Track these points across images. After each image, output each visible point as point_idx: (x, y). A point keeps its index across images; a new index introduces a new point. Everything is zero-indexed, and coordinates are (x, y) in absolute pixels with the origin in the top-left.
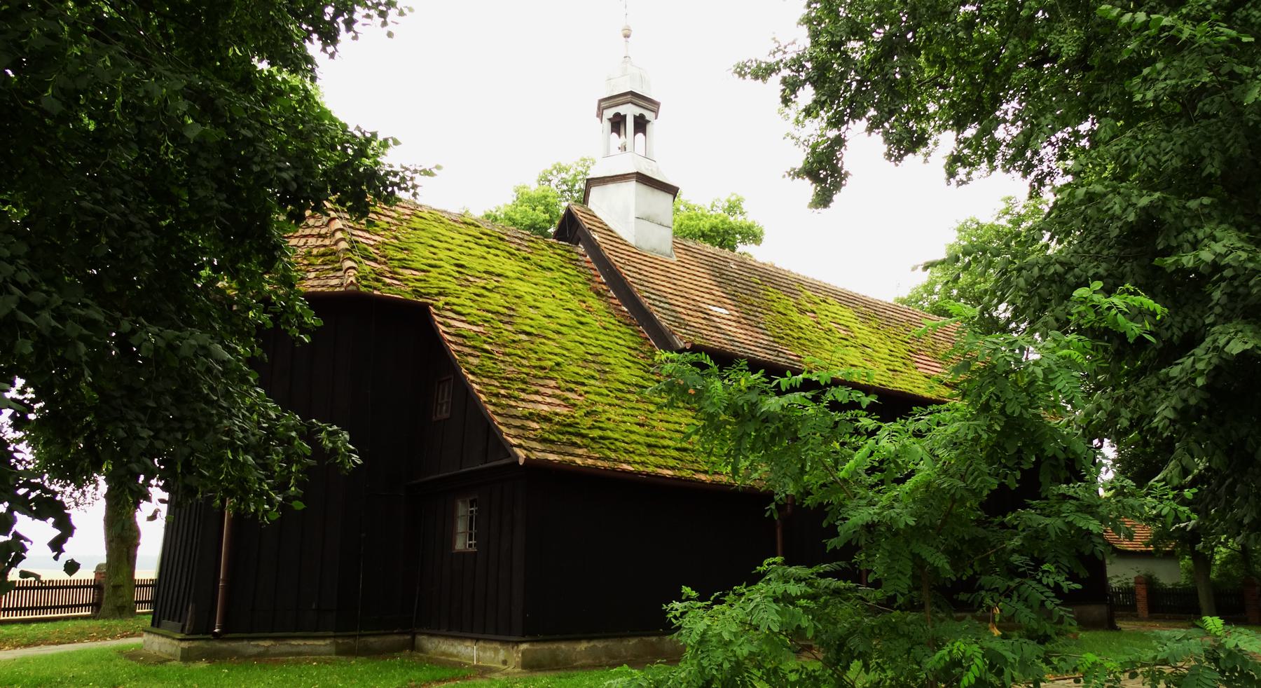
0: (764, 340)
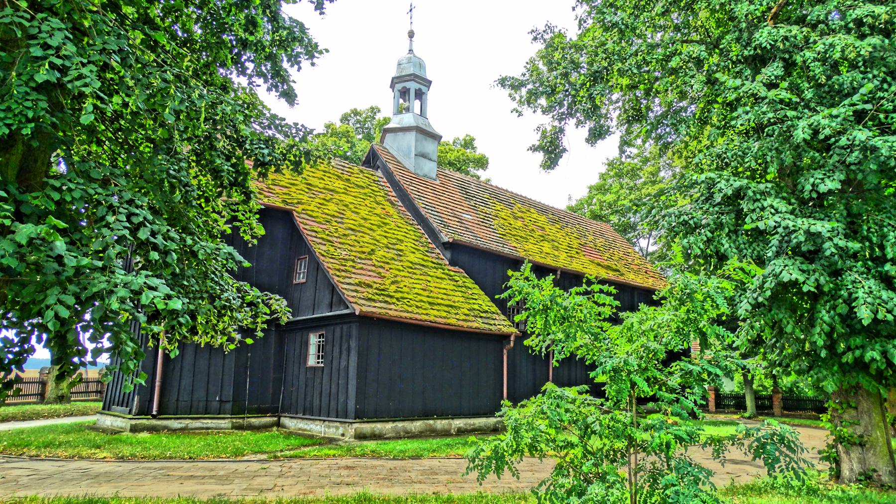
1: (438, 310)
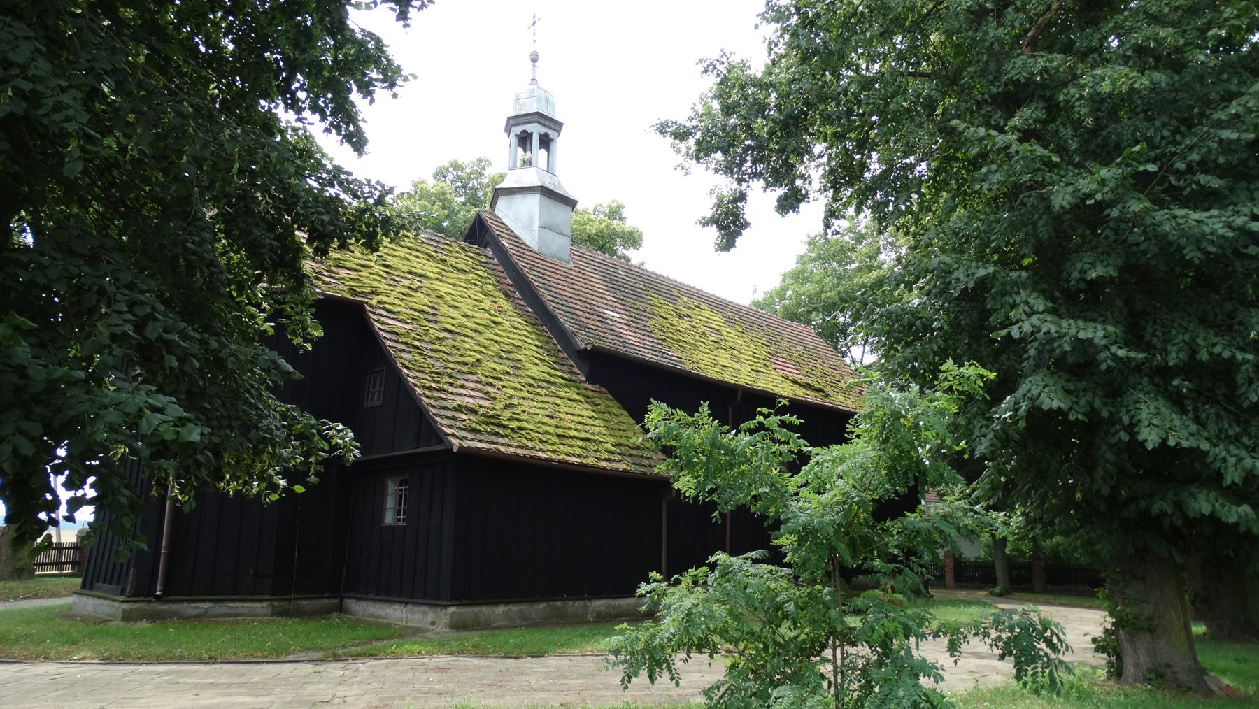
0: (650, 342)
1: (571, 446)
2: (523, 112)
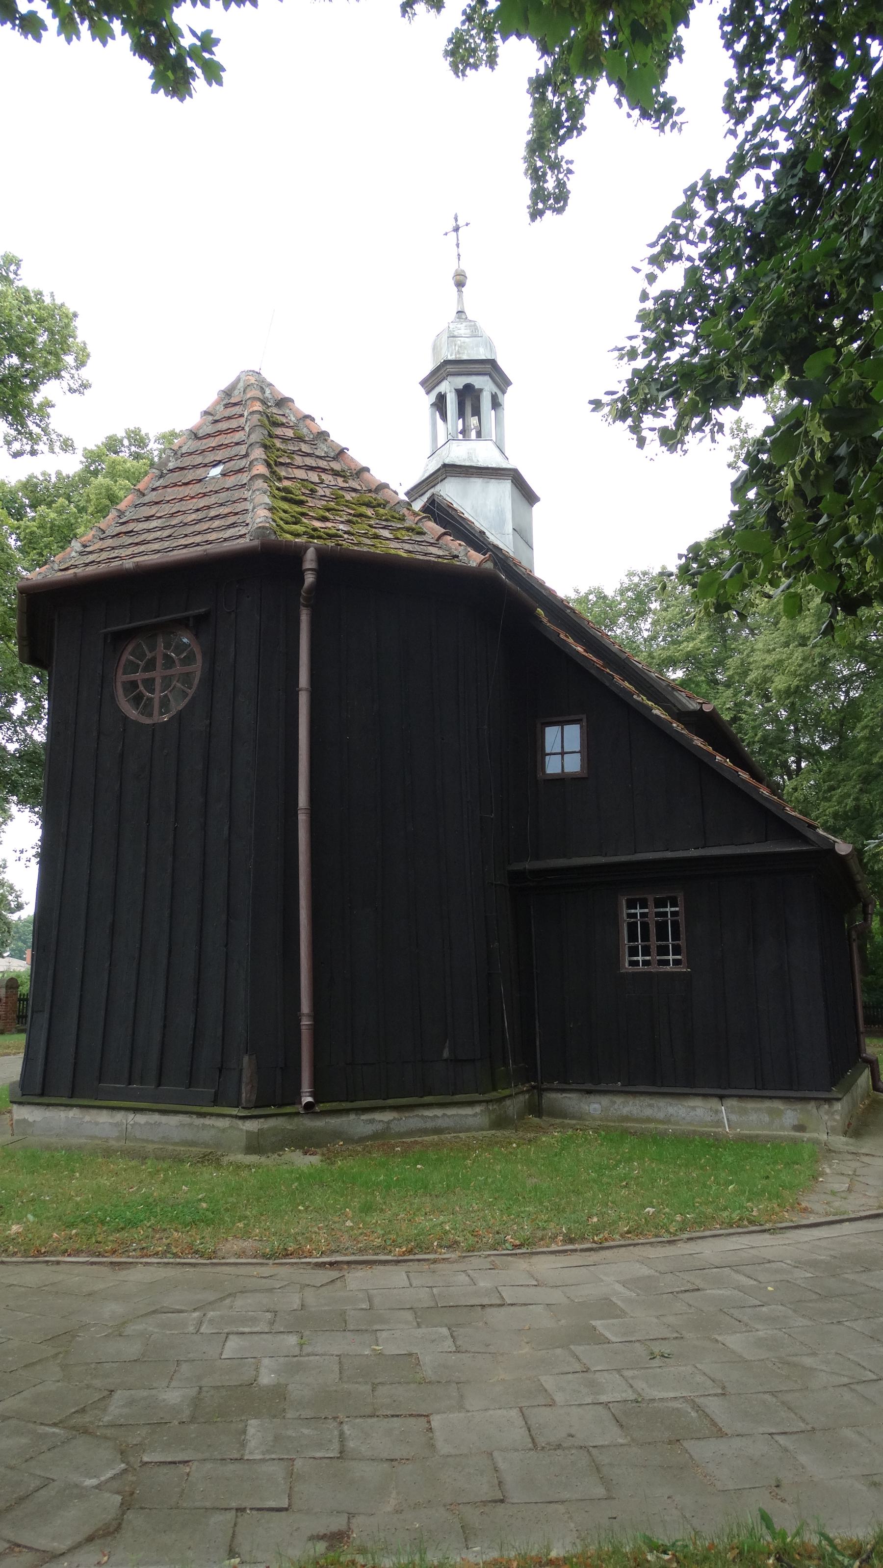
2: (465, 357)
